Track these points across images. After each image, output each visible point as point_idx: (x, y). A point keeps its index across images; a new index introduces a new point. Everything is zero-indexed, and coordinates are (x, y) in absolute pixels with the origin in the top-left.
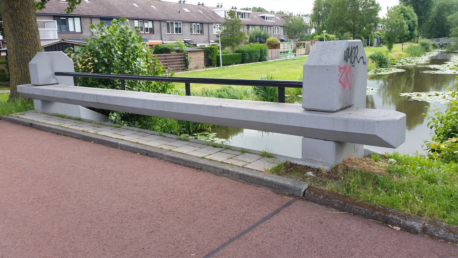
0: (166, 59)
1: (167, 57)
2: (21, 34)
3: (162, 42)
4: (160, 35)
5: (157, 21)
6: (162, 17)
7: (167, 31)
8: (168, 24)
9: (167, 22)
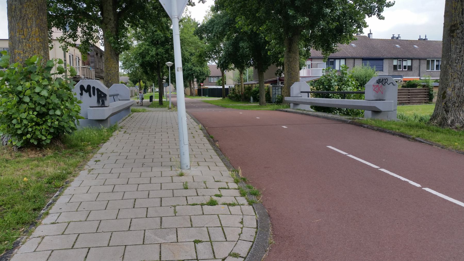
0: (409, 92)
1: (410, 91)
2: (291, 74)
3: (420, 78)
4: (418, 72)
5: (417, 59)
6: (423, 55)
7: (426, 68)
8: (428, 62)
9: (427, 61)
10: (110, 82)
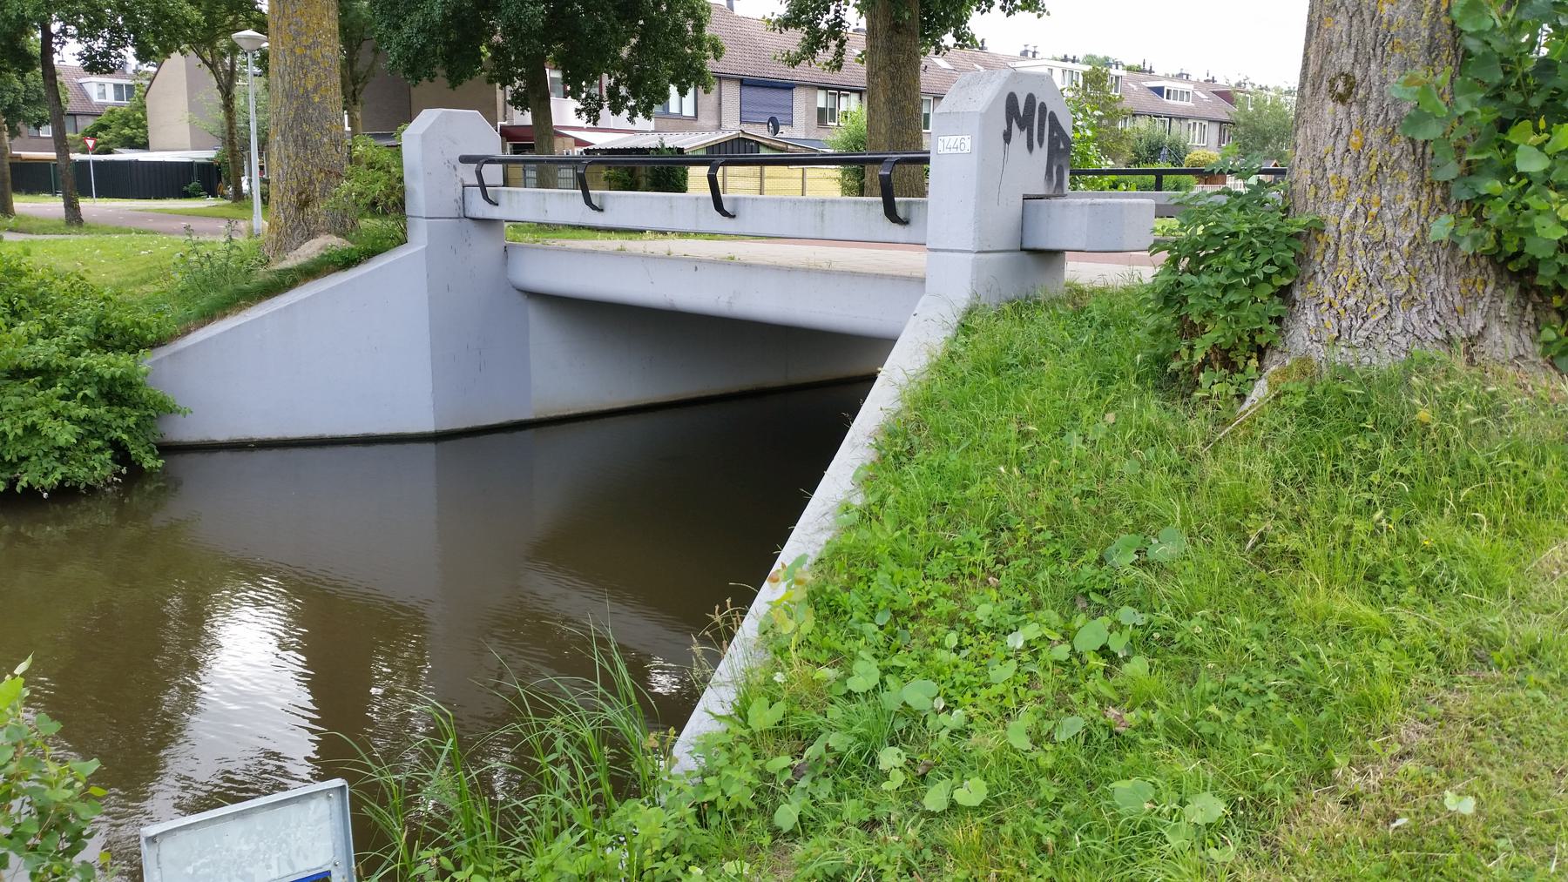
10: (317, 100)
